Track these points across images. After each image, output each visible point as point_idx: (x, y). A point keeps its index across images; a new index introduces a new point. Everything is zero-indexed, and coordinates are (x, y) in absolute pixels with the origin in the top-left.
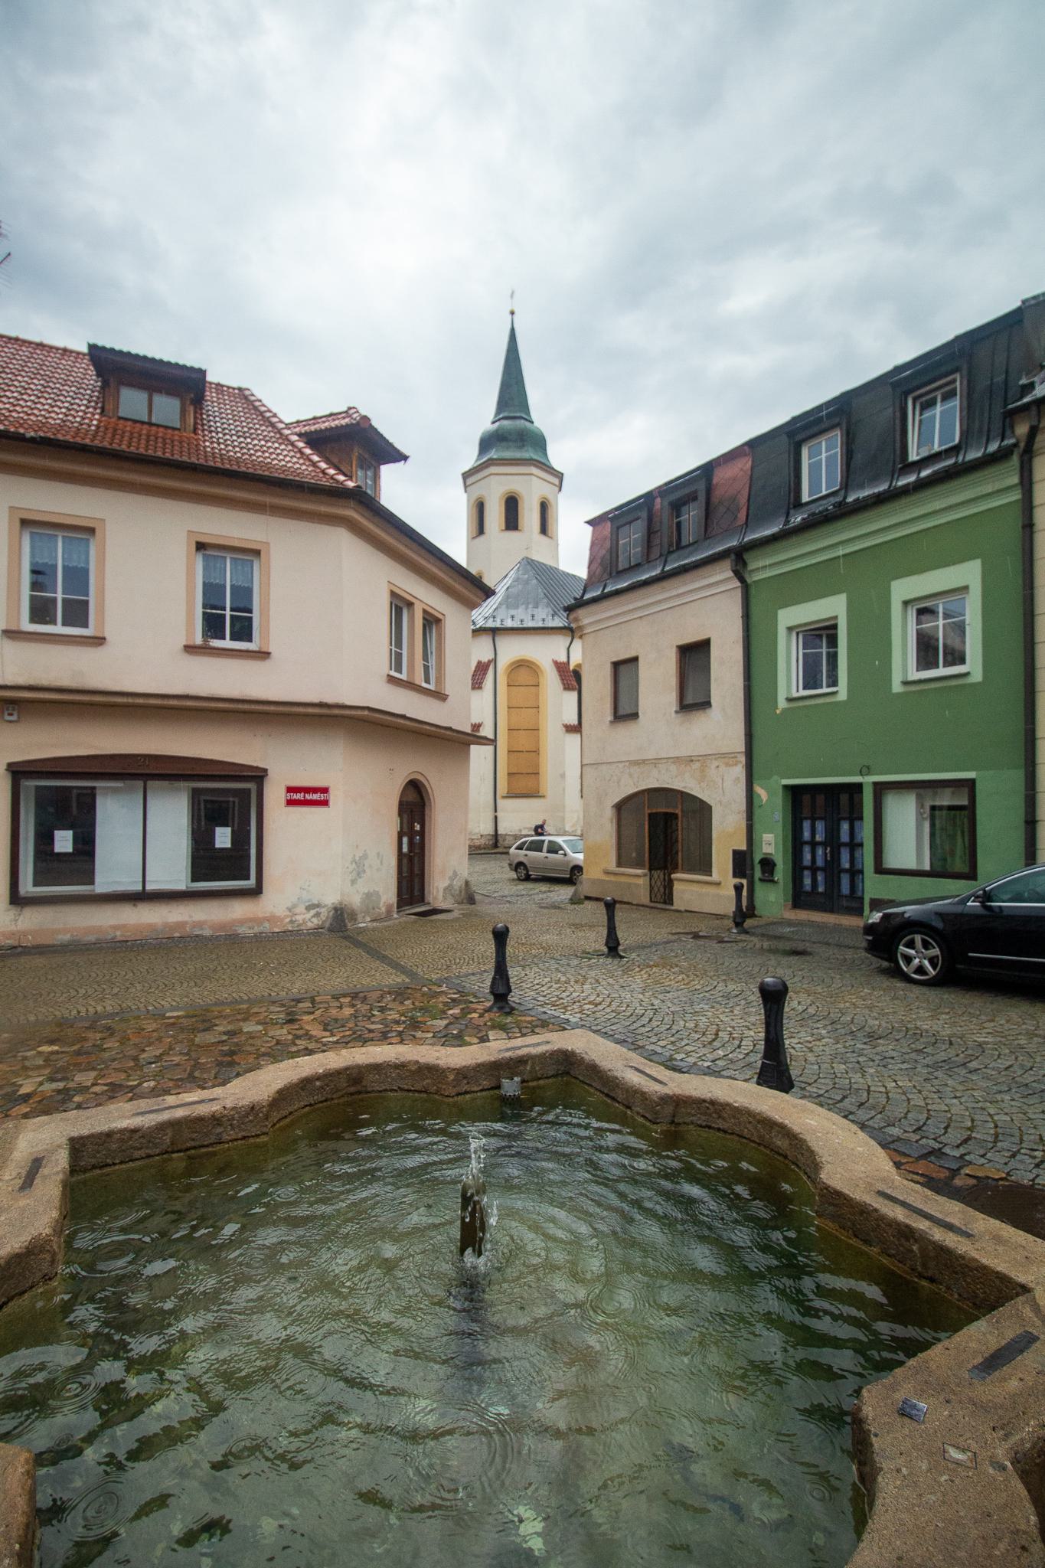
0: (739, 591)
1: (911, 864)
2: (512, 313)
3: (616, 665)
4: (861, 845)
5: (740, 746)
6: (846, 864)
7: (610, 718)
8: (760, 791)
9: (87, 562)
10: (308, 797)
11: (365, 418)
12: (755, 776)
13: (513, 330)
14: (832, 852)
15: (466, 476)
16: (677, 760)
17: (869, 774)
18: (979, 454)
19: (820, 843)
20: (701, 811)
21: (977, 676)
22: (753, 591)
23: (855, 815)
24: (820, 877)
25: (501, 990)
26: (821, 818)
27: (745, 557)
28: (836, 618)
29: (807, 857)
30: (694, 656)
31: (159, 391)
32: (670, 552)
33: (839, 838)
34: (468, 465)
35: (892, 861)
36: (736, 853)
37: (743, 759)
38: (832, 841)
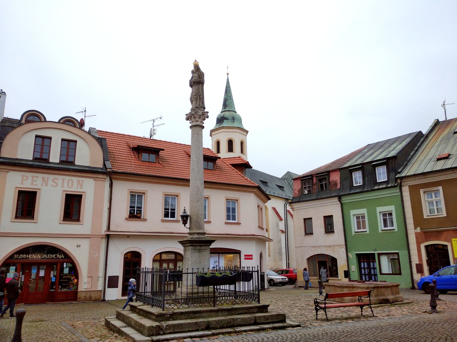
0: (340, 205)
1: (388, 272)
2: (228, 74)
3: (305, 219)
4: (376, 268)
6: (373, 273)
7: (304, 234)
8: (350, 255)
10: (249, 257)
11: (248, 162)
13: (228, 79)
17: (376, 251)
19: (366, 268)
20: (334, 260)
21: (396, 230)
23: (374, 261)
24: (367, 277)
27: (341, 197)
29: (363, 272)
30: (328, 221)
31: (210, 161)
33: (370, 267)
34: (212, 128)
35: (384, 271)
36: (345, 271)
37: (345, 247)
38: (369, 267)
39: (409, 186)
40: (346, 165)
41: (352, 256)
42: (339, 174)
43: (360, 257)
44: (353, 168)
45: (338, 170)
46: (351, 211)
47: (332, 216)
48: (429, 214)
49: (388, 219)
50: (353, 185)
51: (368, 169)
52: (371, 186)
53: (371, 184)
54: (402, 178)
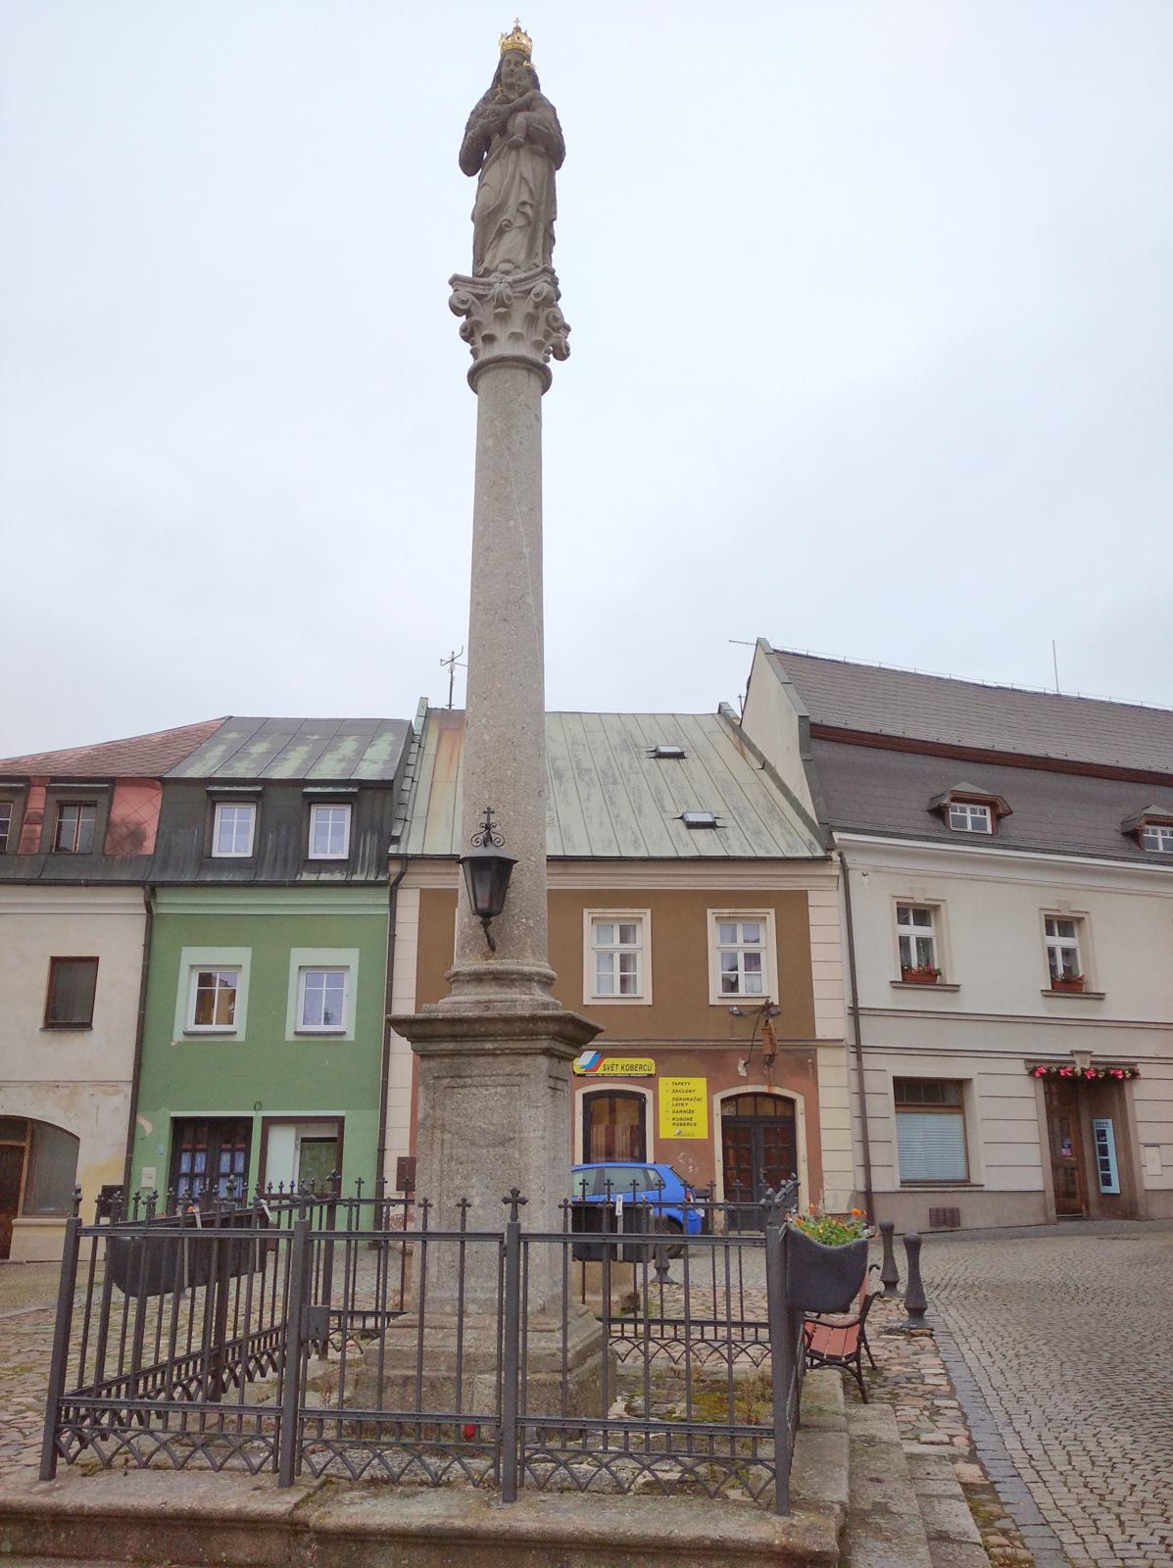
0: (143, 920)
5: (128, 1074)
13: (750, 678)
16: (36, 1084)
18: (343, 878)
21: (241, 1037)
22: (156, 923)
25: (890, 1279)
27: (157, 890)
37: (129, 1089)
39: (422, 890)
40: (195, 771)
41: (156, 1131)
42: (160, 796)
43: (185, 1132)
44: (227, 789)
45: (158, 783)
46: (295, 952)
47: (95, 960)
48: (596, 994)
49: (217, 994)
50: (211, 853)
51: (284, 804)
52: (285, 866)
53: (286, 861)
54: (405, 859)
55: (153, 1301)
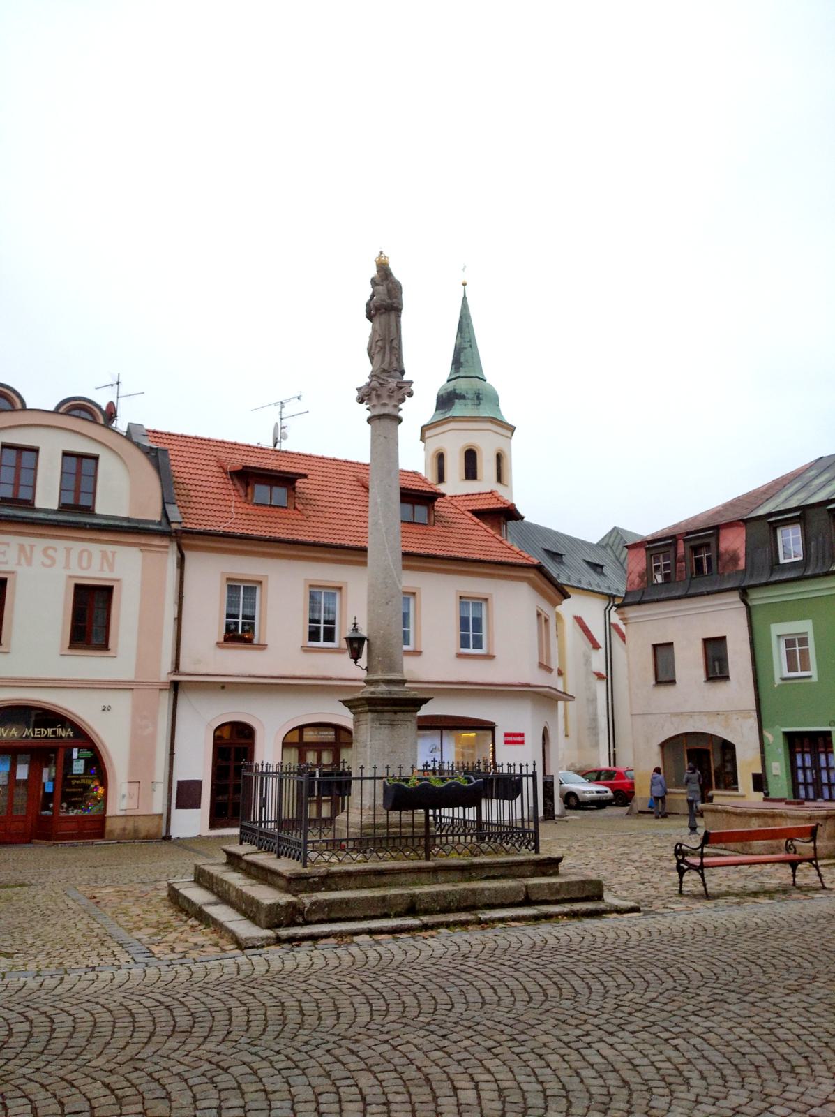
2: (464, 284)
3: (655, 647)
7: (653, 682)
8: (768, 735)
9: (409, 609)
12: (764, 723)
13: (465, 298)
14: (816, 773)
15: (425, 429)
16: (707, 714)
20: (728, 748)
21: (815, 679)
22: (753, 611)
26: (807, 752)
27: (748, 591)
28: (806, 633)
29: (801, 777)
30: (715, 649)
32: (692, 578)
33: (819, 764)
34: (426, 421)
37: (755, 714)
41: (775, 738)
43: (794, 741)
47: (724, 638)
52: (824, 562)
53: (824, 557)
55: (456, 809)
